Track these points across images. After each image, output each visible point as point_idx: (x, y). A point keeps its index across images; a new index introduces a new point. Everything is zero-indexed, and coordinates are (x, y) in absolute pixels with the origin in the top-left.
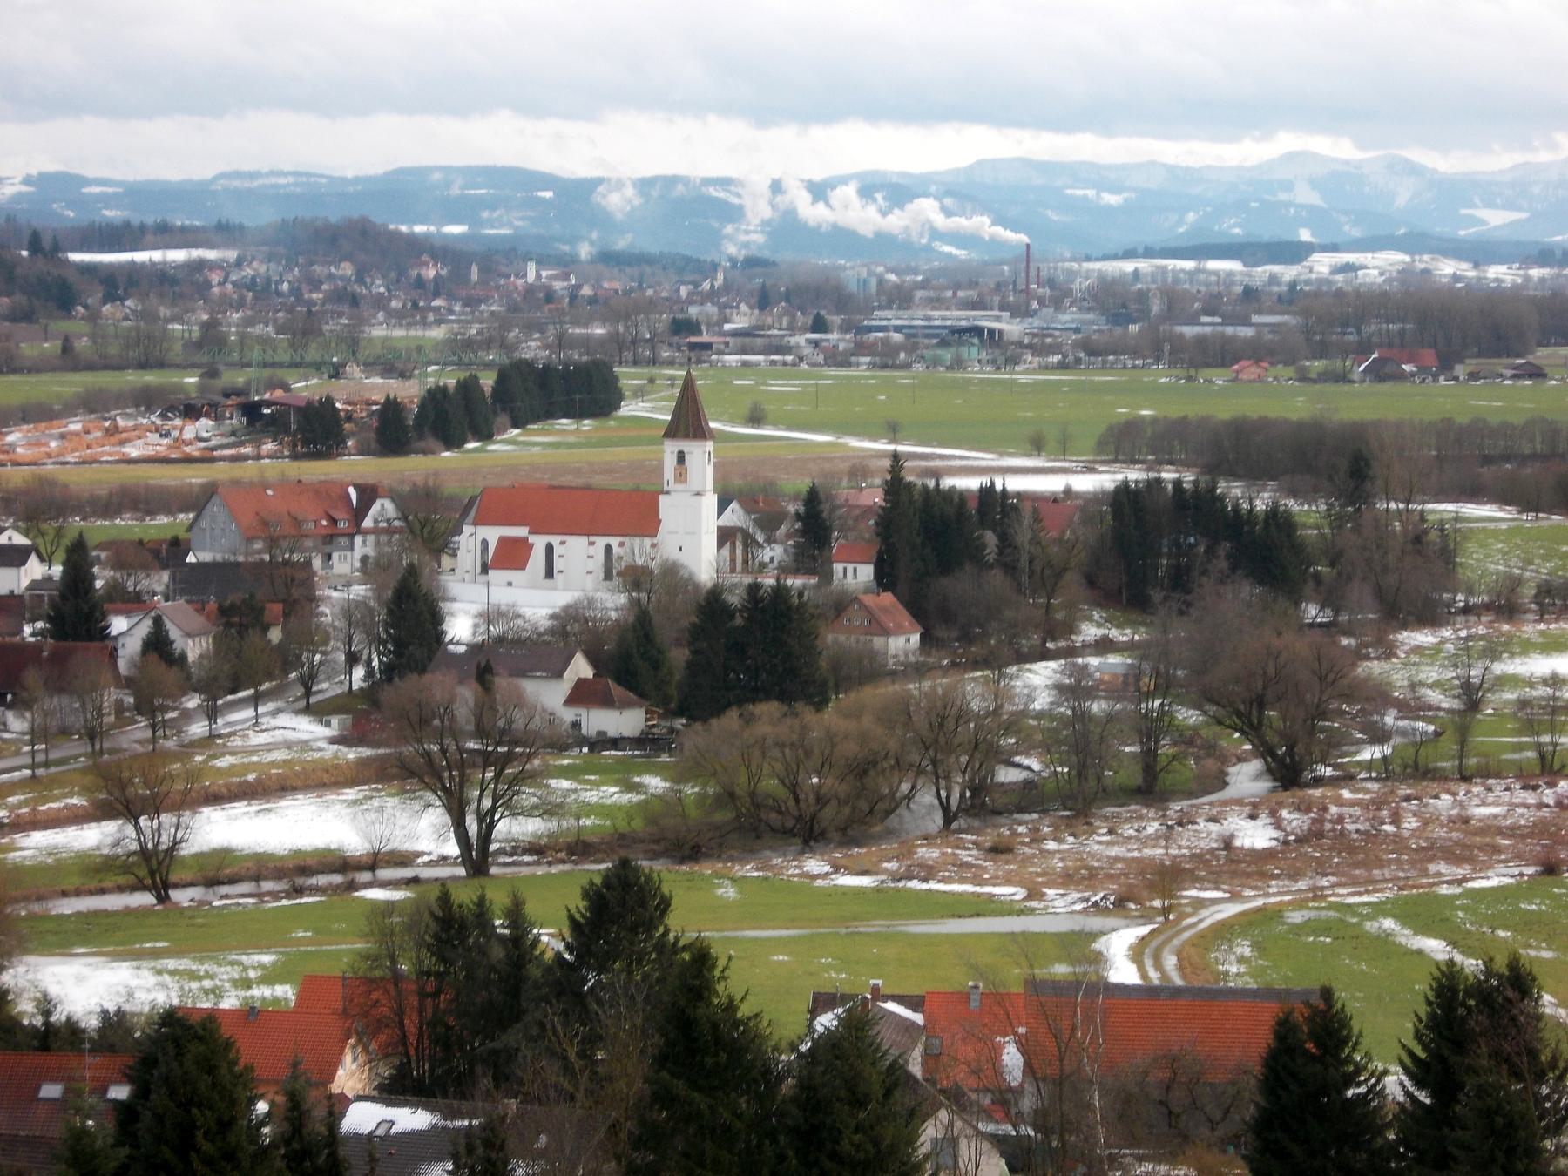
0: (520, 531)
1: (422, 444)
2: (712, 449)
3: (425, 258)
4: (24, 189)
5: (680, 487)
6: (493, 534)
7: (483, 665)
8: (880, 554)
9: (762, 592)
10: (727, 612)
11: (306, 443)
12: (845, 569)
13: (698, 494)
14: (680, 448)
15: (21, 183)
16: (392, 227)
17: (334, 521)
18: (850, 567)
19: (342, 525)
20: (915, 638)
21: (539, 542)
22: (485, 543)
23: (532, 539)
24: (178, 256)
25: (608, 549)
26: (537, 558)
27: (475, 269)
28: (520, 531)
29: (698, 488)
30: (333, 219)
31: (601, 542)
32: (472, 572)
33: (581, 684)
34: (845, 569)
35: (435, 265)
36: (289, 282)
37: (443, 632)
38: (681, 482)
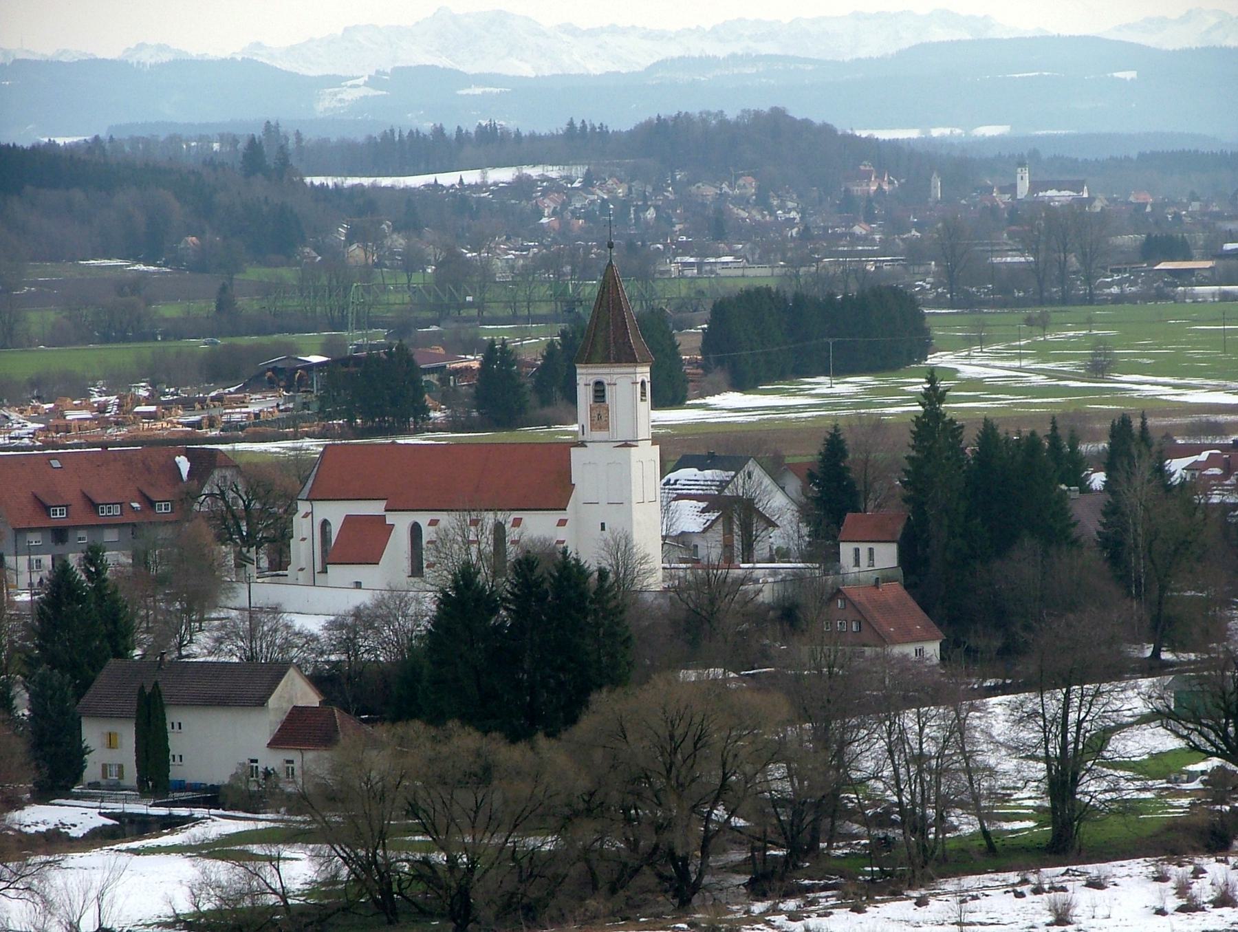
0: (374, 508)
1: (548, 411)
2: (647, 378)
3: (865, 167)
4: (371, 92)
5: (598, 435)
6: (335, 513)
7: (148, 690)
8: (908, 526)
9: (538, 572)
10: (488, 604)
11: (367, 415)
12: (857, 551)
13: (627, 444)
14: (599, 378)
15: (366, 84)
16: (864, 134)
17: (150, 503)
18: (864, 548)
19: (162, 509)
20: (932, 649)
21: (401, 523)
22: (325, 523)
23: (391, 518)
24: (503, 175)
25: (499, 529)
26: (399, 543)
27: (937, 183)
28: (374, 508)
29: (628, 437)
30: (732, 114)
31: (489, 518)
32: (309, 570)
33: (298, 714)
34: (857, 551)
35: (880, 177)
36: (657, 208)
37: (589, 695)
38: (600, 428)
